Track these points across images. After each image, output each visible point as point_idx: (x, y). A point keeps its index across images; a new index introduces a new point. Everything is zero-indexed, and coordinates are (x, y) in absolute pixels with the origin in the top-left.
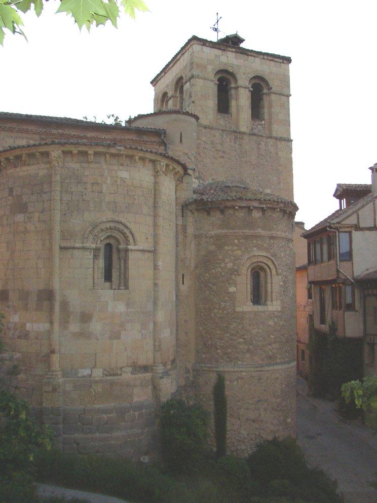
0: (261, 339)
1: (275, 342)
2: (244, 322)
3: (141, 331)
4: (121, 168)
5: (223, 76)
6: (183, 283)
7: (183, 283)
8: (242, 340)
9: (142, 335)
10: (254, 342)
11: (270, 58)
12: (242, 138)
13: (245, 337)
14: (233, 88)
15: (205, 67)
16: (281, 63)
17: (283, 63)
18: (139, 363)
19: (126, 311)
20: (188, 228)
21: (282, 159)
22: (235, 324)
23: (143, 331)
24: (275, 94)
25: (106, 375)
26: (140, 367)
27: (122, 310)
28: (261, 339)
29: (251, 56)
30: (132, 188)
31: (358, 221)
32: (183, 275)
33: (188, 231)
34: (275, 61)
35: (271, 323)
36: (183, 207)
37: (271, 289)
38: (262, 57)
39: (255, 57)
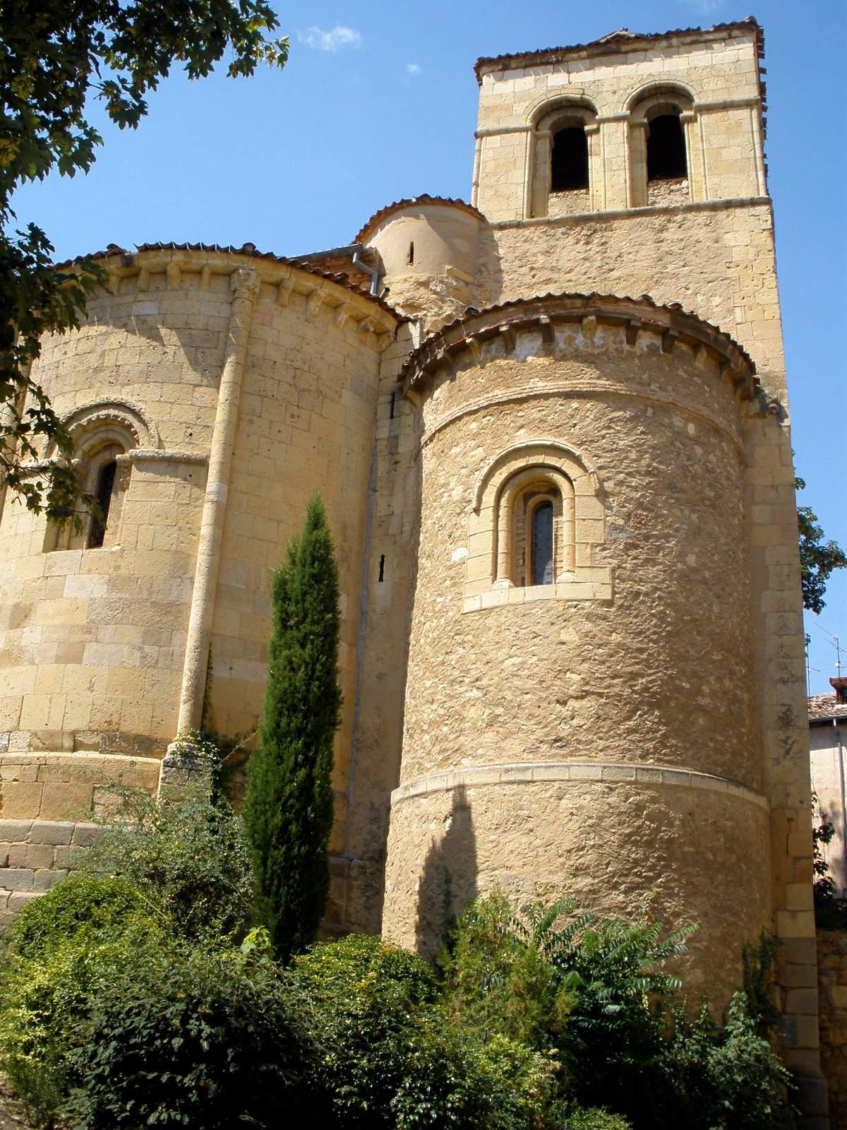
0: (531, 684)
2: (483, 639)
3: (140, 648)
4: (141, 296)
5: (566, 118)
6: (381, 579)
7: (381, 579)
8: (476, 693)
9: (144, 658)
11: (688, 39)
13: (484, 682)
15: (509, 109)
18: (125, 727)
20: (401, 441)
22: (461, 651)
23: (147, 649)
25: (37, 749)
26: (125, 737)
27: (95, 596)
28: (531, 684)
29: (634, 51)
32: (383, 557)
33: (401, 450)
36: (393, 395)
37: (497, 517)
38: (664, 43)
39: (646, 50)
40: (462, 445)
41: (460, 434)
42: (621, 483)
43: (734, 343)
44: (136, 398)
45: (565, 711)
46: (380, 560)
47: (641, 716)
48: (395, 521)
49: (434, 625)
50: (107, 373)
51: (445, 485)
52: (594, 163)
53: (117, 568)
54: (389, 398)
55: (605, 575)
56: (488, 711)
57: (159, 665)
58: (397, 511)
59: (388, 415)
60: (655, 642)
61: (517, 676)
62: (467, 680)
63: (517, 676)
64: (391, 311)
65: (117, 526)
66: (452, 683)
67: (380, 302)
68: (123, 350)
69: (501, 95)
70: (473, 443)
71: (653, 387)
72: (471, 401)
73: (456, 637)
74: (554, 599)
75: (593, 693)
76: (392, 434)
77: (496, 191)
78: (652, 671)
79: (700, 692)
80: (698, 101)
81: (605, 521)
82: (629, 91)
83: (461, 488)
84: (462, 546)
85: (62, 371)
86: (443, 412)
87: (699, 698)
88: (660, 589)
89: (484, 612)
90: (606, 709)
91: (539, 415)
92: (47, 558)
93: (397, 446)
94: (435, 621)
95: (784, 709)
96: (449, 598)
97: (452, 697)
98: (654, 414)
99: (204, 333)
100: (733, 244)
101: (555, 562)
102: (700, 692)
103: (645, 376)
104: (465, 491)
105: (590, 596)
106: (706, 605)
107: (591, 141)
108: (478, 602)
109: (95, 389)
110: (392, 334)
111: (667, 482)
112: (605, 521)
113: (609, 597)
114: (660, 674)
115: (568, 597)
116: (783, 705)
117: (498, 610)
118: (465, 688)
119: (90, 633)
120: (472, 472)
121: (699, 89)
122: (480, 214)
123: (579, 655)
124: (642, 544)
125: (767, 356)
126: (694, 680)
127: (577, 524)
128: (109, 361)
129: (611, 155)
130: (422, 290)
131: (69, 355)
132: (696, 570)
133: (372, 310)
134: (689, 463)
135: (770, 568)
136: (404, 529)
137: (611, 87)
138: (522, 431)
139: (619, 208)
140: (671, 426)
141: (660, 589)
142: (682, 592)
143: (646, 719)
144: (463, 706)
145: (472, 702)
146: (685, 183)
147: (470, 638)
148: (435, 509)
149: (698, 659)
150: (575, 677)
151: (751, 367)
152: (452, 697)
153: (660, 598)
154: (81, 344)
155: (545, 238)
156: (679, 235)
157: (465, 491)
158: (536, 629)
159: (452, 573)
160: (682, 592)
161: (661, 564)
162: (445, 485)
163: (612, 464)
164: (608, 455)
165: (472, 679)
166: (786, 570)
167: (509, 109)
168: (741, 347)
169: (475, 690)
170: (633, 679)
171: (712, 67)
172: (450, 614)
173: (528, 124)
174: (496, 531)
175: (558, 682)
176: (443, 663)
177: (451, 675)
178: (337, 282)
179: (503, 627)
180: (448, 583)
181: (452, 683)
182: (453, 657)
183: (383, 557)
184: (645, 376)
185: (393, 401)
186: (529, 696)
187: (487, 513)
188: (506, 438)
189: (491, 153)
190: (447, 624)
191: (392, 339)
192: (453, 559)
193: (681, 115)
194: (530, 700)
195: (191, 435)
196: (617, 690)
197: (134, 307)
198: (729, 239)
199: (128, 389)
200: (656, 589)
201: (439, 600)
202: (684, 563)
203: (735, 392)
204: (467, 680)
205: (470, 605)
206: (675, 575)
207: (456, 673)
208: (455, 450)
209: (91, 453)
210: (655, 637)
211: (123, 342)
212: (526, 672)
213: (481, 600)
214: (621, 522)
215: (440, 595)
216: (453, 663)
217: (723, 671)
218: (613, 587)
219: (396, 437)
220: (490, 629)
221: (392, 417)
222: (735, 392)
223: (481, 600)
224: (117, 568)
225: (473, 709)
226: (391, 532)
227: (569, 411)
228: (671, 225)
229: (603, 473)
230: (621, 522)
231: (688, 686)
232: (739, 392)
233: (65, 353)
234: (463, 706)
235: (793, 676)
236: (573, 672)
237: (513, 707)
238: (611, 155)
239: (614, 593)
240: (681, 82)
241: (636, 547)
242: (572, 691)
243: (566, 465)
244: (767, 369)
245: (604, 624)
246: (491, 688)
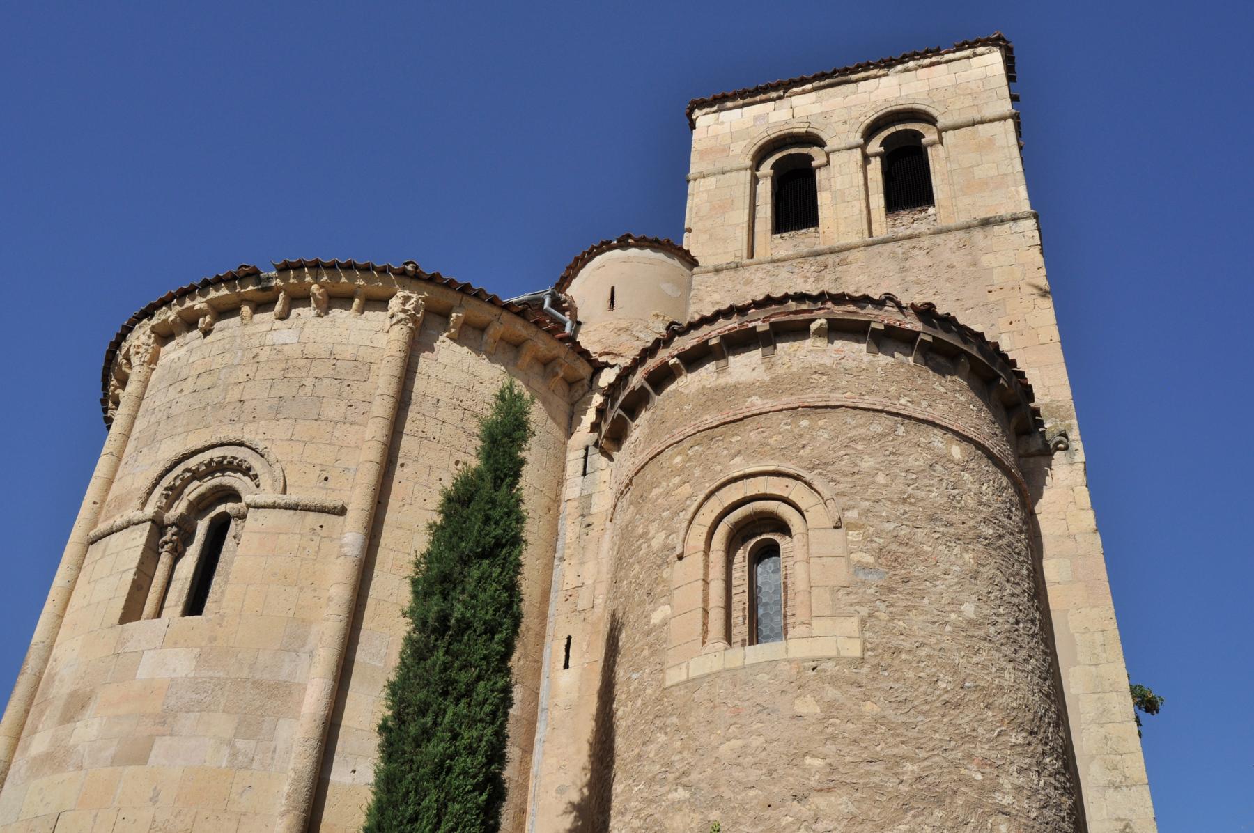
0: (754, 774)
1: (827, 789)
2: (692, 720)
3: (230, 743)
6: (566, 666)
7: (566, 666)
8: (682, 794)
9: (234, 755)
10: (728, 794)
12: (844, 263)
13: (694, 776)
14: (820, 167)
15: (725, 150)
16: (969, 57)
17: (975, 55)
19: (192, 675)
21: (995, 271)
22: (662, 738)
23: (240, 744)
24: (955, 128)
28: (754, 774)
30: (301, 362)
31: (856, 147)
32: (569, 638)
33: (594, 510)
34: (947, 62)
35: (808, 706)
36: (587, 449)
40: (664, 484)
41: (661, 473)
42: (866, 513)
43: (1005, 356)
44: (261, 436)
45: (804, 810)
46: (565, 642)
47: (914, 817)
48: (585, 595)
49: (628, 709)
50: (229, 410)
51: (645, 534)
52: (823, 199)
53: (213, 639)
54: (582, 453)
55: (852, 626)
56: (698, 817)
57: (254, 766)
58: (589, 582)
59: (581, 471)
60: (925, 714)
61: (739, 765)
62: (670, 777)
63: (739, 765)
64: (585, 354)
65: (222, 592)
66: (651, 782)
67: (572, 340)
68: (251, 384)
69: (716, 137)
70: (676, 480)
71: (903, 401)
72: (675, 432)
73: (657, 721)
74: (785, 660)
75: (844, 784)
76: (585, 493)
77: (711, 235)
78: (926, 755)
79: (998, 788)
80: (942, 121)
81: (849, 560)
82: (862, 119)
83: (662, 535)
84: (664, 604)
85: (175, 410)
86: (643, 450)
87: (998, 796)
88: (929, 645)
89: (692, 684)
90: (865, 807)
91: (759, 437)
92: (122, 630)
93: (589, 507)
94: (630, 704)
95: (1121, 826)
96: (647, 671)
97: (649, 802)
98: (906, 432)
99: (352, 364)
100: (994, 265)
101: (785, 616)
102: (998, 788)
103: (893, 389)
104: (667, 537)
105: (833, 653)
106: (994, 670)
107: (820, 176)
108: (684, 670)
109: (211, 429)
110: (586, 382)
111: (929, 512)
112: (849, 560)
113: (858, 654)
114: (937, 759)
115: (802, 656)
116: (1118, 819)
117: (709, 679)
118: (667, 788)
119: (164, 723)
120: (677, 513)
121: (942, 109)
122: (692, 257)
123: (821, 732)
124: (901, 586)
125: (1047, 384)
126: (988, 770)
127: (813, 557)
128: (234, 395)
129: (848, 188)
130: (624, 337)
131: (186, 392)
132: (977, 624)
133: (561, 350)
134: (956, 491)
135: (1078, 637)
136: (597, 602)
137: (837, 113)
138: (738, 459)
139: (854, 239)
140: (928, 447)
141: (929, 645)
142: (959, 650)
143: (924, 822)
144: (665, 812)
145: (676, 806)
146: (931, 210)
147: (674, 719)
148: (632, 565)
149: (989, 740)
150: (818, 762)
151: (1028, 392)
152: (649, 802)
153: (929, 656)
154: (201, 379)
155: (768, 279)
156: (927, 261)
157: (667, 537)
158: (760, 700)
159: (651, 639)
160: (959, 650)
161: (928, 613)
162: (645, 534)
163: (854, 490)
164: (849, 479)
165: (677, 774)
166: (1099, 638)
167: (725, 150)
168: (1014, 363)
169: (680, 790)
170: (898, 764)
171: (957, 85)
172: (649, 691)
173: (749, 163)
174: (706, 582)
175: (795, 771)
176: (639, 757)
177: (649, 771)
178: (518, 314)
179: (717, 701)
180: (646, 653)
181: (651, 782)
182: (652, 747)
183: (569, 638)
184: (893, 389)
185: (586, 457)
186: (752, 793)
187: (695, 561)
188: (718, 468)
189: (705, 196)
190: (645, 704)
191: (586, 388)
192: (652, 621)
193: (923, 140)
194: (756, 797)
195: (326, 479)
196: (876, 780)
197: (269, 336)
198: (986, 260)
199: (252, 427)
200: (923, 644)
201: (634, 676)
202: (960, 613)
203: (1009, 422)
204: (670, 777)
205: (674, 676)
206: (948, 628)
207: (657, 768)
208: (656, 491)
209: (200, 507)
210: (926, 707)
211: (251, 375)
212: (750, 759)
213: (687, 668)
214: (871, 560)
215: (636, 670)
216: (651, 755)
217: (1027, 760)
218: (864, 642)
219: (590, 496)
220: (700, 704)
221: (584, 474)
222: (1009, 422)
223: (687, 668)
224: (213, 639)
225: (678, 817)
226: (580, 607)
227: (796, 431)
228: (917, 251)
229: (843, 501)
230: (871, 560)
231: (979, 777)
232: (1014, 421)
233: (182, 391)
234: (665, 812)
235: (1126, 778)
236: (814, 756)
237: (734, 808)
238: (848, 188)
239: (864, 650)
240: (921, 104)
241: (892, 590)
242: (814, 781)
243: (796, 492)
244: (1047, 399)
245: (854, 690)
246: (702, 785)
